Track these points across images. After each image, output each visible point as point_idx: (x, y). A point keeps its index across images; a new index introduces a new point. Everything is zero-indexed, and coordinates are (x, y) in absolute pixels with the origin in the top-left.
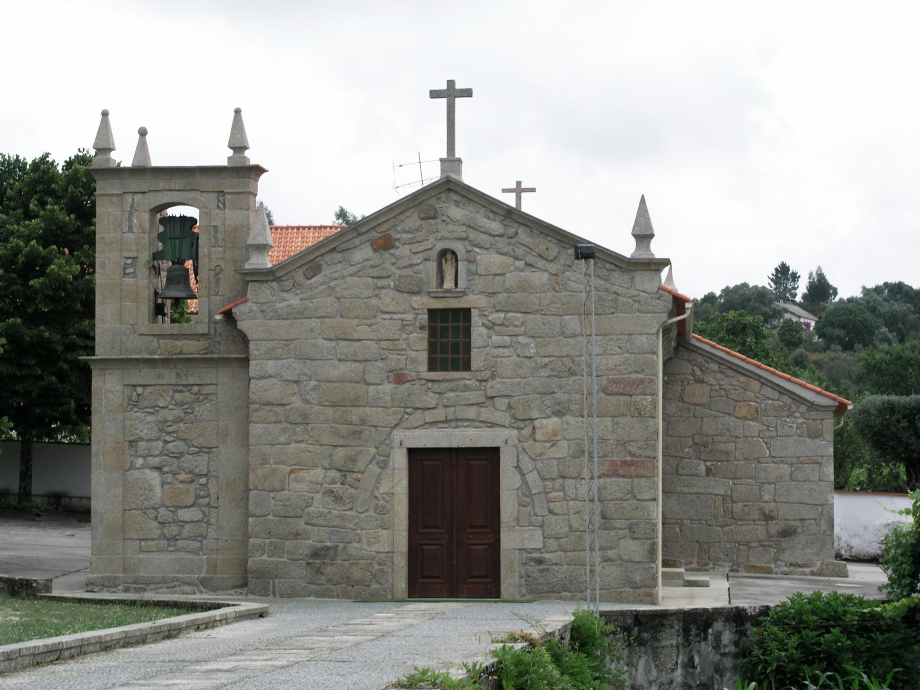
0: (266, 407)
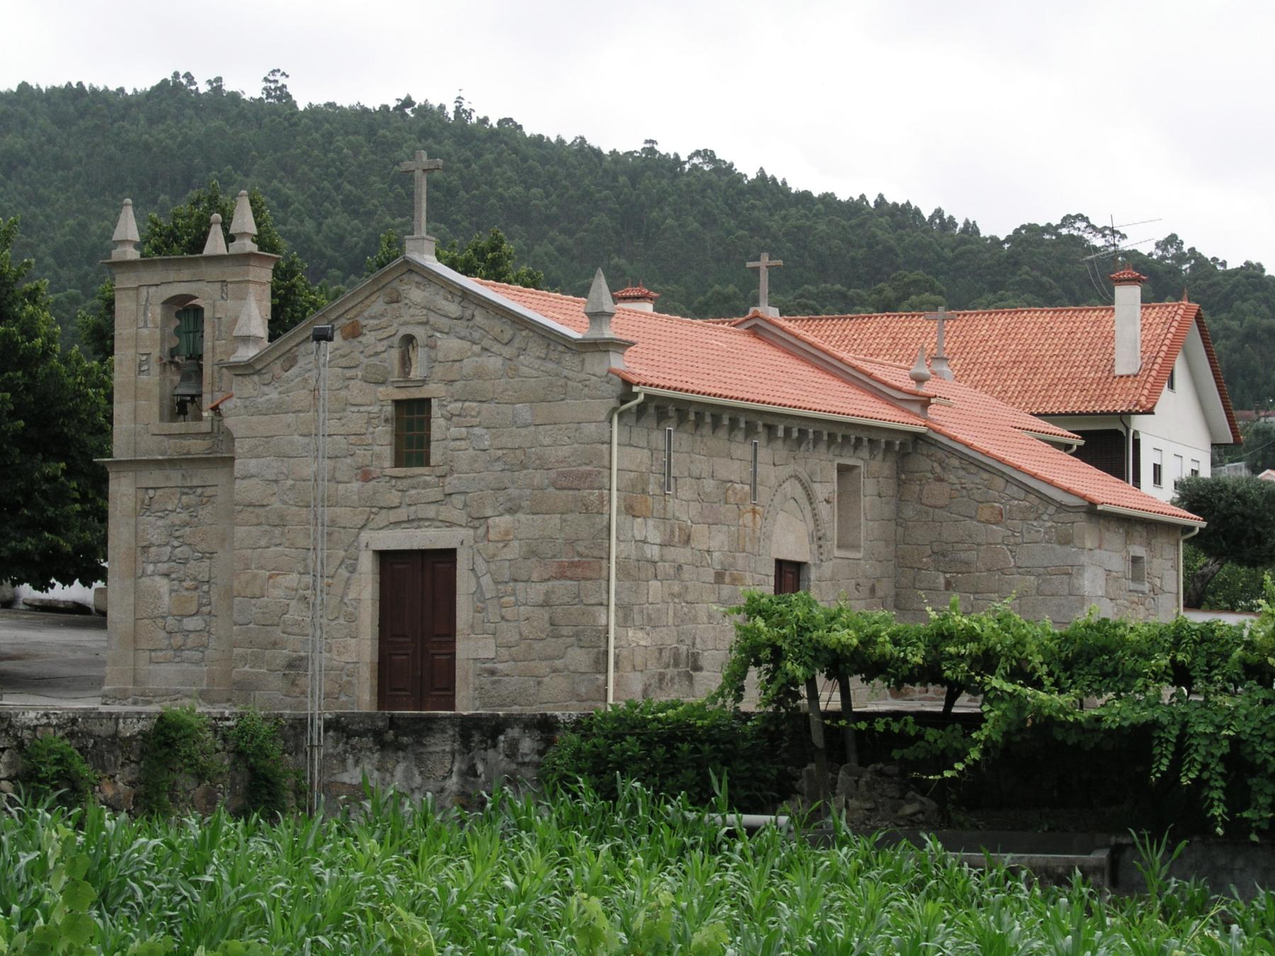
0: (250, 509)
